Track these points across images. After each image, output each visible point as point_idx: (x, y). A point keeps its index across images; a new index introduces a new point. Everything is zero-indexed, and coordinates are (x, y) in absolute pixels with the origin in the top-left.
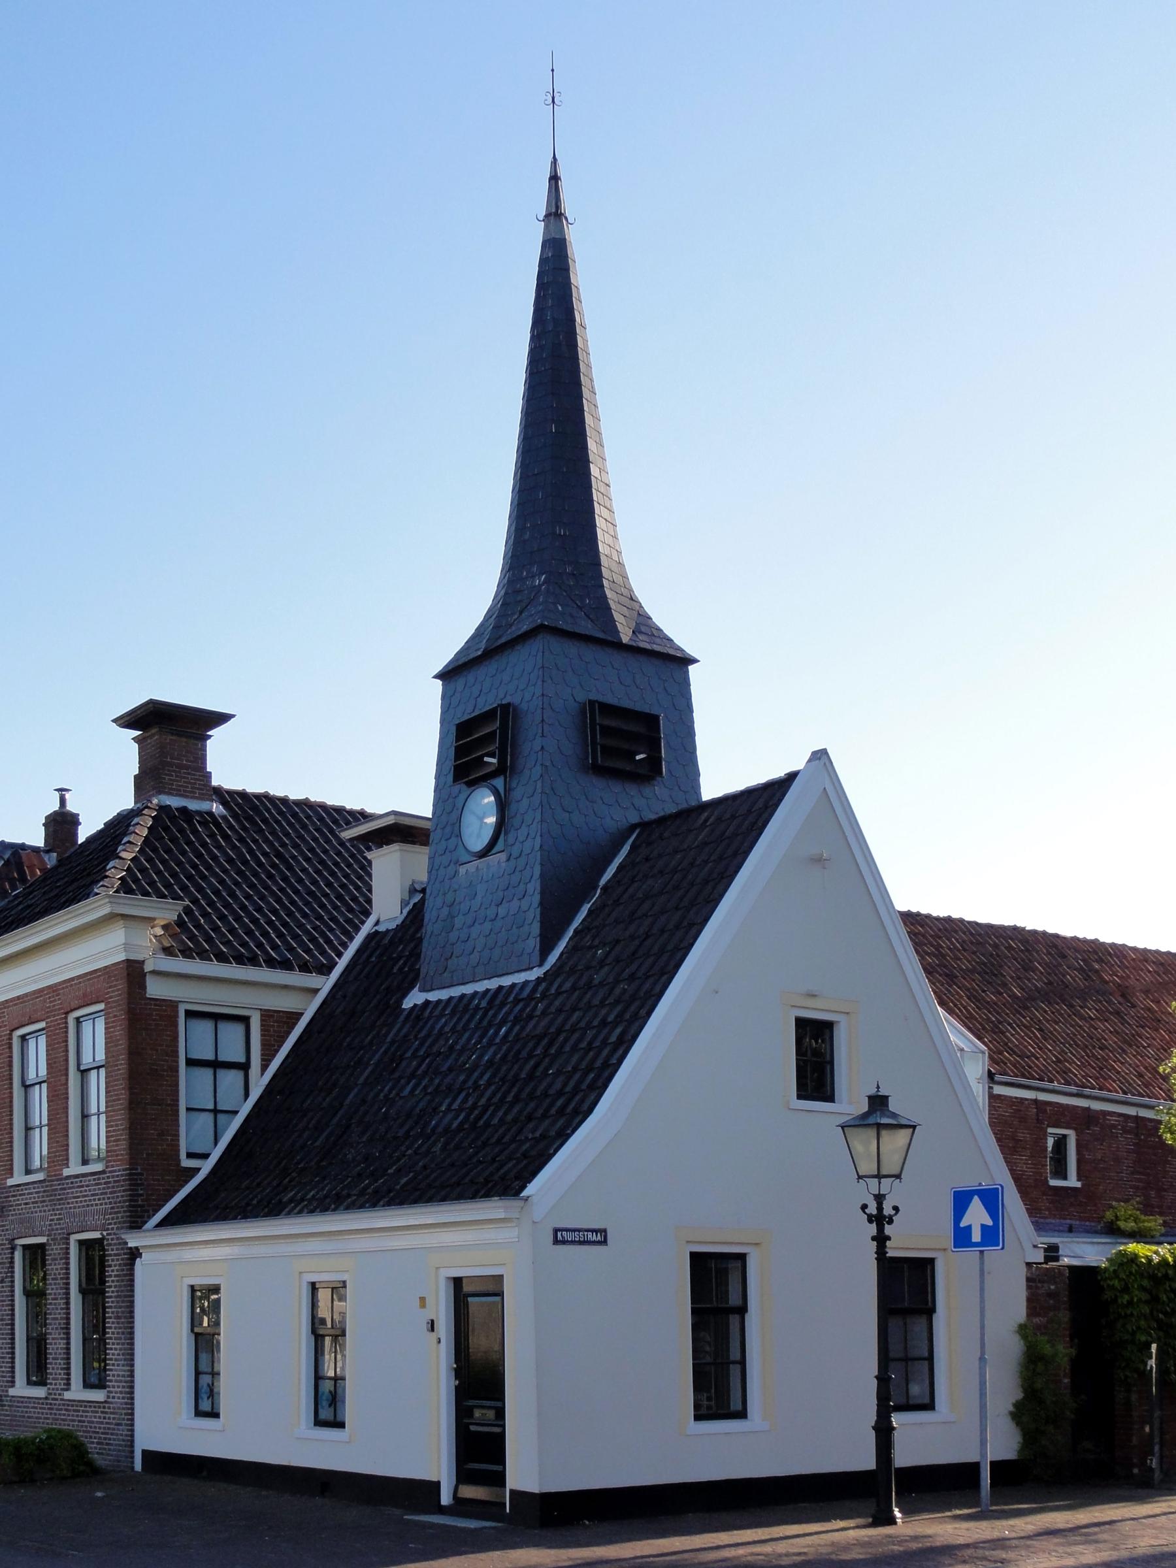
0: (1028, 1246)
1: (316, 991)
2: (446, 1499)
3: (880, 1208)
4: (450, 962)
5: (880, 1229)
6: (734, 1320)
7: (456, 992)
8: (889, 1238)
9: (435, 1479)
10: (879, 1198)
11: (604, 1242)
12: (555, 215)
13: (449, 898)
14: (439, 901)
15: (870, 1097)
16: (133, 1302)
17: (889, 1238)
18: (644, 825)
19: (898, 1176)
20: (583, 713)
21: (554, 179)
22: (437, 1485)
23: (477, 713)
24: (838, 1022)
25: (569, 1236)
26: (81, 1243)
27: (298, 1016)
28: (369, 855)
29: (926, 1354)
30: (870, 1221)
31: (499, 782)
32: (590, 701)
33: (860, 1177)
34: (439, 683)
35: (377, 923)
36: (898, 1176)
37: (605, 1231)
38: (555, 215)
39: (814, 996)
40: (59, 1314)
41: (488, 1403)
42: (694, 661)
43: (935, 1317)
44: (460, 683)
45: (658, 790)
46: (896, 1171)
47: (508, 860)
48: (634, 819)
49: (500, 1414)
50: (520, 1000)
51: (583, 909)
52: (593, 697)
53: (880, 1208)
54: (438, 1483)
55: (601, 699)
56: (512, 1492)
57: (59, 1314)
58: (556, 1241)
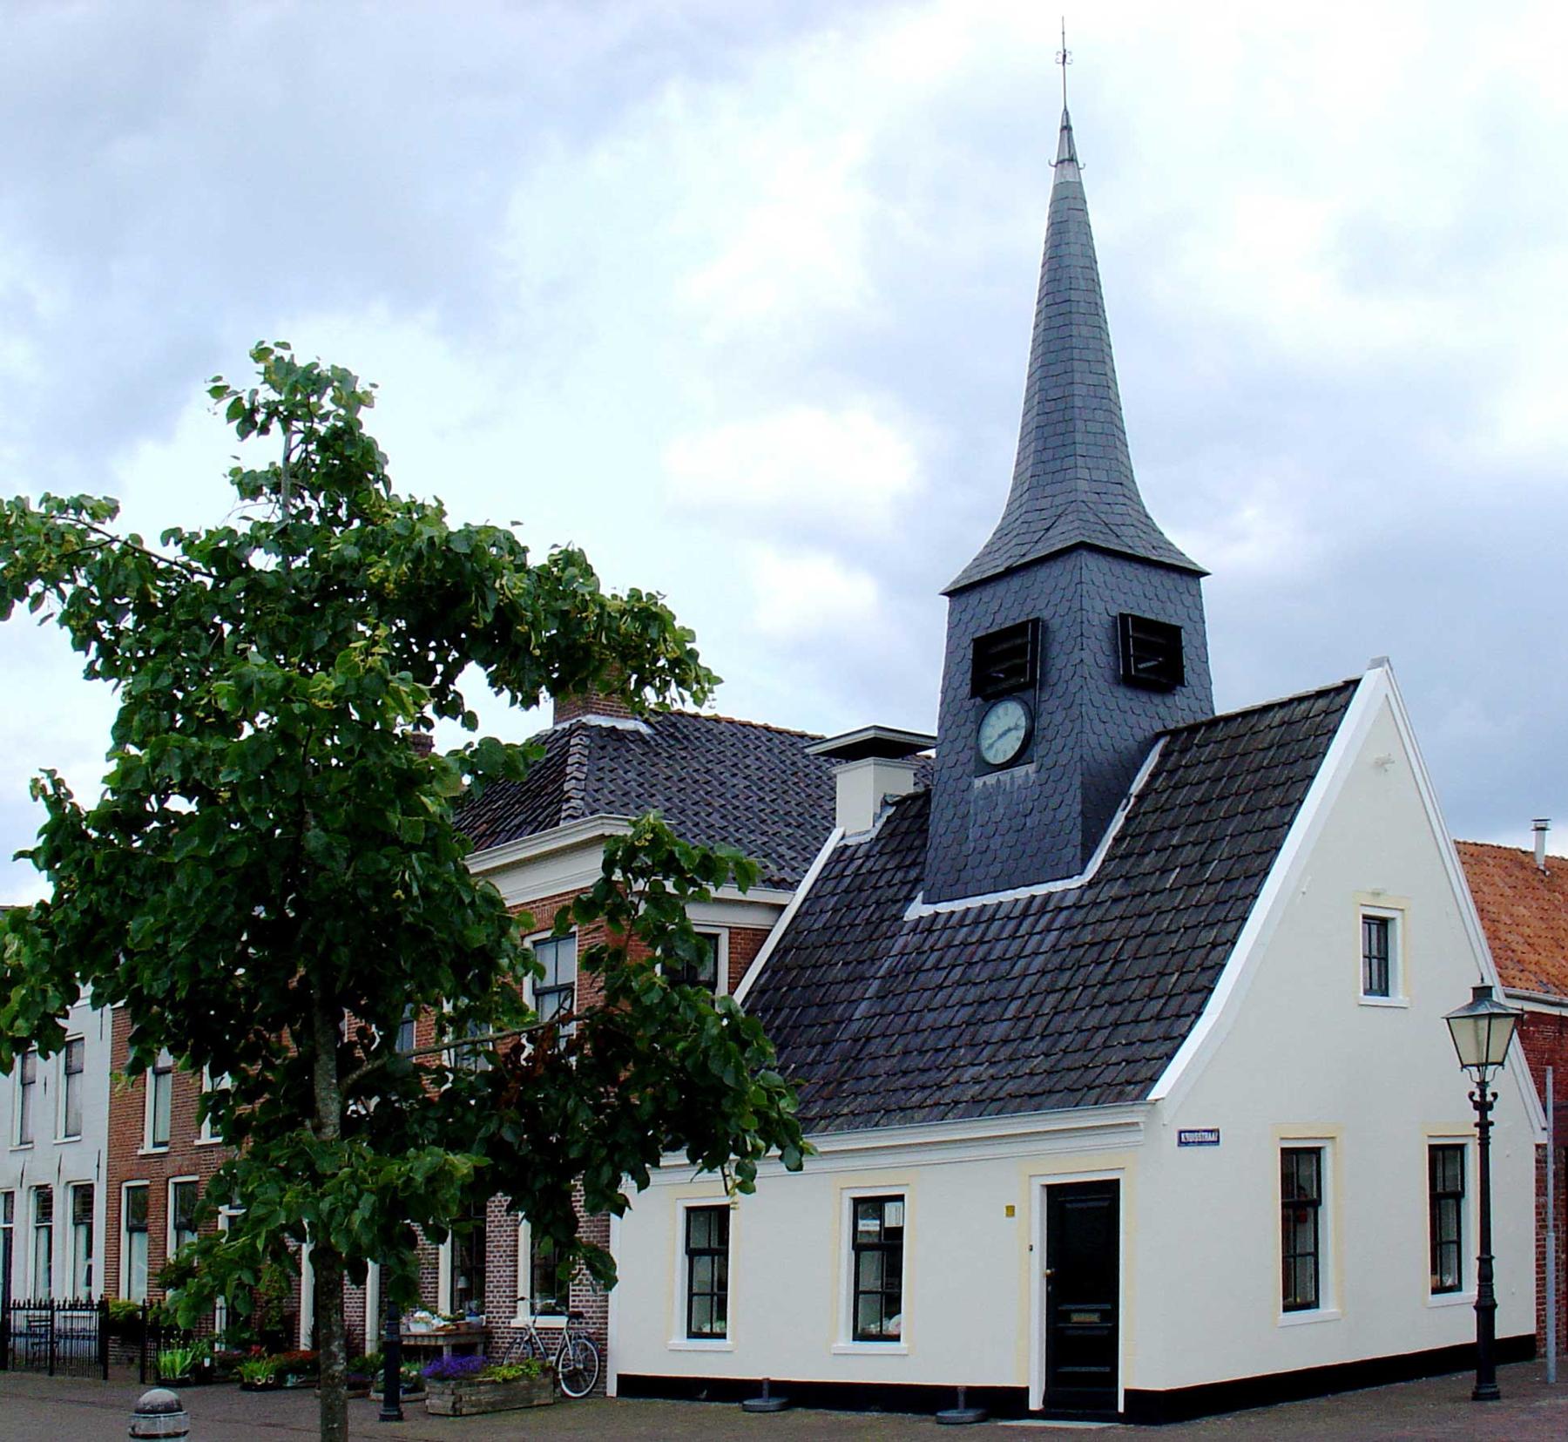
0: (1537, 1127)
1: (781, 909)
2: (1035, 1403)
3: (1483, 1095)
4: (963, 874)
5: (1483, 1116)
6: (1311, 1211)
7: (975, 902)
8: (1492, 1124)
9: (1023, 1385)
10: (1483, 1085)
11: (1217, 1142)
12: (1068, 159)
13: (962, 809)
14: (949, 814)
15: (1475, 989)
16: (608, 1226)
17: (1492, 1124)
18: (1174, 734)
19: (1501, 1064)
20: (1115, 625)
21: (1066, 128)
22: (1024, 1392)
23: (995, 629)
24: (1393, 919)
25: (1190, 1137)
26: (129, 1188)
27: (765, 933)
28: (834, 771)
29: (695, 1298)
30: (1475, 1108)
31: (1028, 695)
32: (1121, 614)
33: (1464, 1066)
34: (947, 599)
35: (843, 837)
36: (1501, 1064)
37: (1218, 1131)
38: (1068, 159)
39: (1378, 894)
40: (505, 1241)
41: (1095, 1307)
42: (719, 681)
43: (1320, 1210)
44: (963, 600)
45: (1180, 699)
46: (1500, 1060)
47: (1038, 771)
48: (1159, 728)
49: (1112, 1316)
50: (1061, 909)
51: (1117, 816)
52: (1126, 611)
53: (1483, 1095)
54: (1026, 1390)
55: (1138, 613)
56: (1127, 1392)
57: (505, 1241)
58: (1181, 1143)
